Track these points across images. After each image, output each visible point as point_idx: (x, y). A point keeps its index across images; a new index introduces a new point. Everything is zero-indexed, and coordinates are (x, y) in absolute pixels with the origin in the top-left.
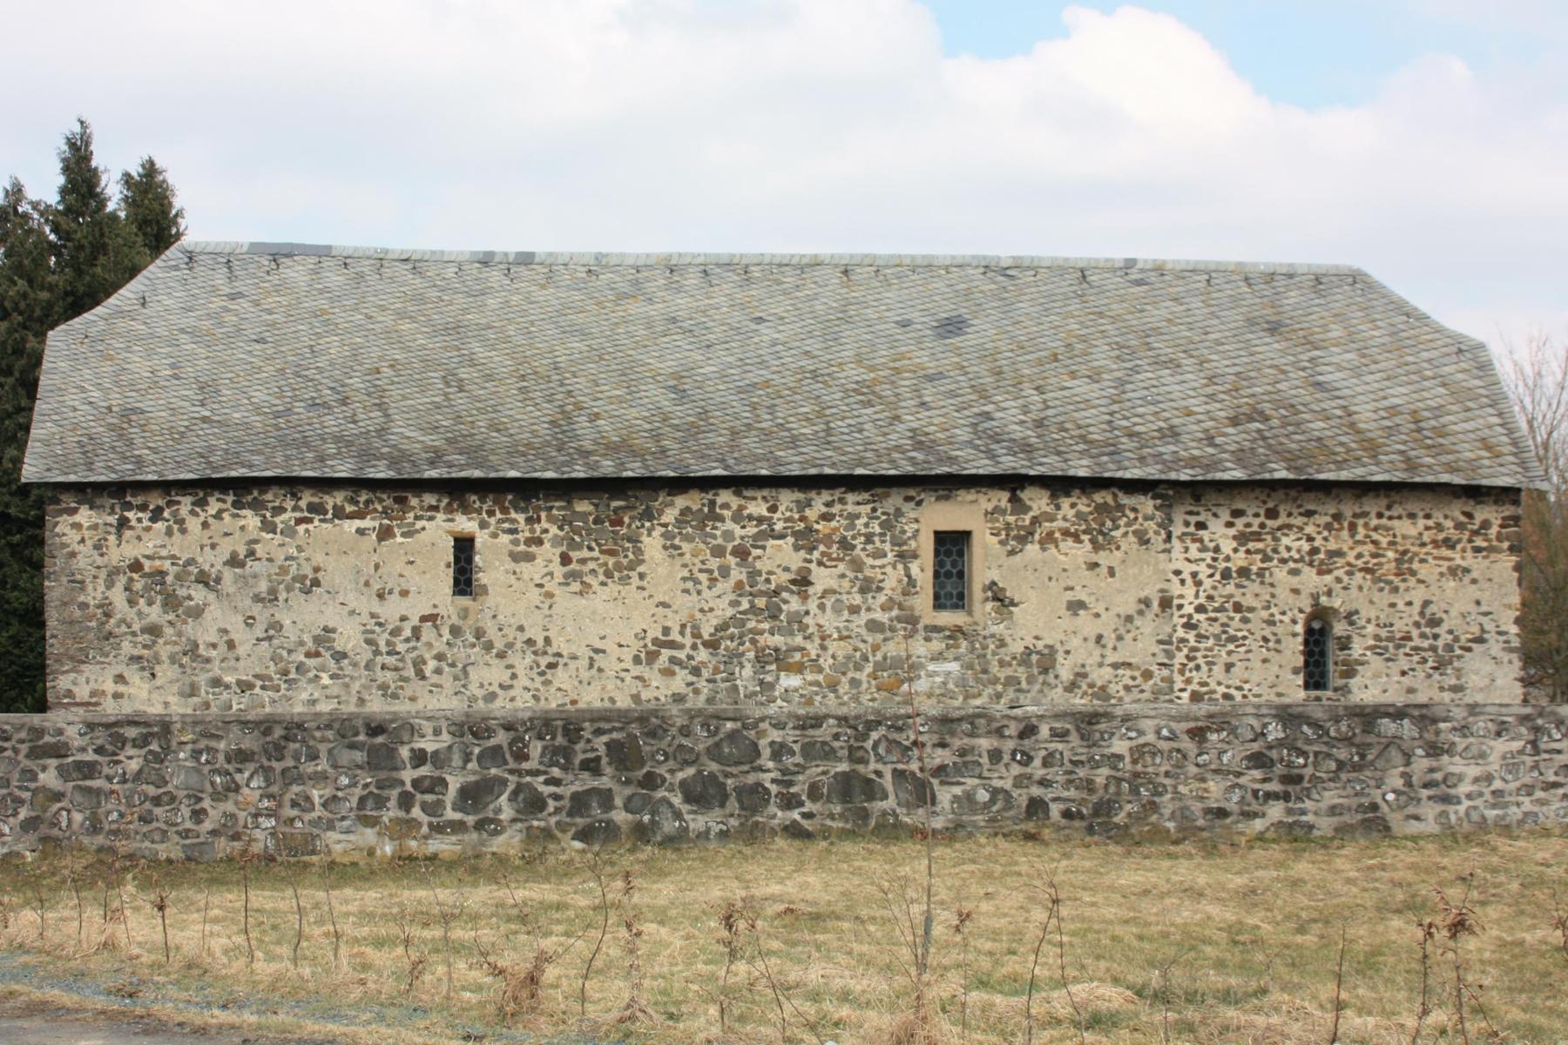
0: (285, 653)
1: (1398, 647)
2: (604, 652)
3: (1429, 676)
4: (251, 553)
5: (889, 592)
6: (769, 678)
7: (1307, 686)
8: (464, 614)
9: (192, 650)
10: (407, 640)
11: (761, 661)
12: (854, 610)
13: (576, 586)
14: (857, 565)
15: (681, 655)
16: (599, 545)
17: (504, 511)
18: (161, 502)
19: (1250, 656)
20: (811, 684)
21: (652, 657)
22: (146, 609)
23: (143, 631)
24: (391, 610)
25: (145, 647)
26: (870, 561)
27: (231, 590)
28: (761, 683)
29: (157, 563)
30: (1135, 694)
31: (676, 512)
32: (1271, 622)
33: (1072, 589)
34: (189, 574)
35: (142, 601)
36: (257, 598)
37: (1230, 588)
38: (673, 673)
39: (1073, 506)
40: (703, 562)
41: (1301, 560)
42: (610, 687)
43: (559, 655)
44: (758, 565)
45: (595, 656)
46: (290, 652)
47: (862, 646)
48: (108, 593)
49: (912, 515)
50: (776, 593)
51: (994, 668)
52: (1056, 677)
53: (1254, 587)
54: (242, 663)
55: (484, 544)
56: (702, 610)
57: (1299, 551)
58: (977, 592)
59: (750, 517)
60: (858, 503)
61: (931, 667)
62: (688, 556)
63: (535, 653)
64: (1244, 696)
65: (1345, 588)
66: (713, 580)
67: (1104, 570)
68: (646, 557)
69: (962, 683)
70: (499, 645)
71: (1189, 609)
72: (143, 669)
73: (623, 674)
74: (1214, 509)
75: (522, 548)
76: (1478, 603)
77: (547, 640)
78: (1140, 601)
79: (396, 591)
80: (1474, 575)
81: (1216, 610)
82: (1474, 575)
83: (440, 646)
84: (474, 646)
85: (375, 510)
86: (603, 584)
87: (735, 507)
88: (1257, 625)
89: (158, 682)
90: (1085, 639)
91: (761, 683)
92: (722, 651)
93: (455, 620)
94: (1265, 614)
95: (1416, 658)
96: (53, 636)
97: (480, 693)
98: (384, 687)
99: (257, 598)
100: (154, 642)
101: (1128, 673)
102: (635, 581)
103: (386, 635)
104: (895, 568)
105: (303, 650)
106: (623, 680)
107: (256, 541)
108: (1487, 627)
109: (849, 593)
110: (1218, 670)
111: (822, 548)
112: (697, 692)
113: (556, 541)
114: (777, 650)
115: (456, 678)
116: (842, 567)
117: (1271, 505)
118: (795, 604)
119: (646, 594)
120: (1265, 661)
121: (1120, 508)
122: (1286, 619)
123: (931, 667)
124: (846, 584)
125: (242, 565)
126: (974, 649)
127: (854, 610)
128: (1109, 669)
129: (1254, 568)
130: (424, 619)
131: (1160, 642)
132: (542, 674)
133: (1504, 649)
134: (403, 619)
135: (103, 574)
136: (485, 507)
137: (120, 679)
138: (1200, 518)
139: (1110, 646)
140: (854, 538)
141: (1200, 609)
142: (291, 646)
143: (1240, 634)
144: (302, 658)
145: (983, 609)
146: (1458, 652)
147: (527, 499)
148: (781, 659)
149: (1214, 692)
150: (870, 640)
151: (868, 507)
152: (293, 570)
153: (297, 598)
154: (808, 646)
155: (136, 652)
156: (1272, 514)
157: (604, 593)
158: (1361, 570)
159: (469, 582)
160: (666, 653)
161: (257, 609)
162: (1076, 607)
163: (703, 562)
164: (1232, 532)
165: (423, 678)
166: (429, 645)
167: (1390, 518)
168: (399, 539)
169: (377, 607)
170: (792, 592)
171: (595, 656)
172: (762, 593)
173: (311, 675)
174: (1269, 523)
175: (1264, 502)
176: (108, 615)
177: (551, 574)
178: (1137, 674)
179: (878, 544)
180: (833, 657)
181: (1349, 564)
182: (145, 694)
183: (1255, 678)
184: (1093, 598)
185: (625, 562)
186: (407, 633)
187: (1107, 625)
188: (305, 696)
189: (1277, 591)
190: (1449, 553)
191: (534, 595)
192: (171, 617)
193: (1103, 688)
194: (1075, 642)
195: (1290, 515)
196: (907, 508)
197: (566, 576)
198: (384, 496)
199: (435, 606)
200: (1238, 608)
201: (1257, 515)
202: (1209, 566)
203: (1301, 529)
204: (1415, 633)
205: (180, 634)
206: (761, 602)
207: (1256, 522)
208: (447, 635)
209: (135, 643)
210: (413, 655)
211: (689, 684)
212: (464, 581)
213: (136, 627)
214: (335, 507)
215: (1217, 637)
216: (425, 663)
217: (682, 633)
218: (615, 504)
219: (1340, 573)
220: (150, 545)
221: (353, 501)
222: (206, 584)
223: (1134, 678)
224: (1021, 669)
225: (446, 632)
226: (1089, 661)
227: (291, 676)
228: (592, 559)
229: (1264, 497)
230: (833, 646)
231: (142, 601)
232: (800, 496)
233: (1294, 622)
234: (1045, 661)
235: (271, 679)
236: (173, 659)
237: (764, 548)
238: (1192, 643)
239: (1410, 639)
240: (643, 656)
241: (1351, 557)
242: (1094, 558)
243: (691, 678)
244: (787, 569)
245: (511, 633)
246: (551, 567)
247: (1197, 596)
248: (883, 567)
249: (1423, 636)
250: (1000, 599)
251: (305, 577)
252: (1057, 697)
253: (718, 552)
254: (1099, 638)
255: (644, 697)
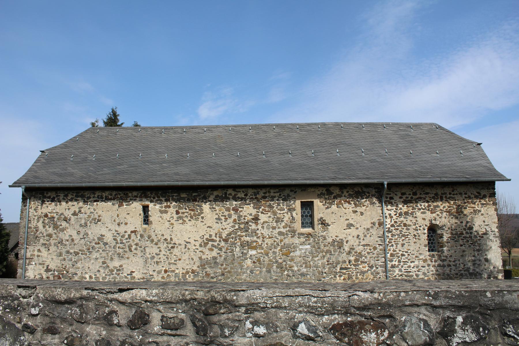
0: (89, 243)
1: (459, 237)
2: (190, 243)
3: (470, 246)
4: (80, 211)
5: (286, 222)
6: (245, 251)
7: (429, 251)
8: (145, 230)
9: (61, 242)
10: (127, 239)
11: (242, 246)
12: (274, 228)
13: (181, 221)
14: (275, 213)
15: (216, 244)
16: (188, 208)
17: (158, 197)
18: (55, 196)
19: (410, 241)
20: (259, 253)
21: (206, 244)
22: (48, 229)
23: (47, 236)
24: (121, 229)
25: (47, 241)
26: (279, 212)
27: (73, 223)
28: (242, 253)
29: (52, 214)
30: (371, 255)
31: (214, 197)
32: (416, 230)
33: (348, 220)
34: (61, 218)
35: (47, 226)
36: (81, 225)
37: (402, 219)
38: (213, 250)
39: (347, 192)
40: (223, 213)
41: (425, 209)
42: (192, 254)
43: (175, 244)
44: (241, 214)
45: (187, 244)
46: (90, 242)
47: (277, 240)
48: (38, 224)
49: (293, 196)
50: (247, 223)
51: (322, 247)
52: (344, 250)
53: (410, 218)
54: (76, 246)
55: (151, 208)
56: (222, 229)
57: (424, 206)
58: (316, 222)
59: (238, 198)
60: (275, 193)
61: (301, 247)
62: (218, 211)
63: (167, 243)
64: (409, 255)
65: (440, 218)
66: (226, 219)
67: (359, 213)
68: (204, 211)
69: (311, 253)
70: (156, 240)
71: (388, 226)
72: (46, 248)
73: (196, 250)
74: (396, 193)
75: (164, 209)
76: (484, 222)
77: (171, 239)
78: (372, 223)
79: (124, 223)
80: (482, 212)
81: (398, 226)
82: (482, 212)
83: (137, 241)
84: (148, 241)
85: (118, 197)
86: (190, 220)
87: (233, 195)
88: (411, 231)
89: (50, 252)
90: (353, 237)
91: (242, 253)
92: (229, 242)
93: (142, 232)
94: (414, 227)
95: (465, 240)
96: (21, 237)
97: (149, 256)
98: (119, 254)
99: (81, 225)
100: (50, 239)
101: (369, 248)
102: (200, 219)
103: (120, 237)
104: (287, 214)
105: (94, 242)
106: (196, 252)
107: (82, 208)
108: (488, 230)
109: (272, 222)
110: (399, 246)
111: (263, 207)
112: (221, 256)
113: (174, 207)
114: (247, 242)
115: (142, 251)
116: (269, 213)
117: (414, 191)
118: (253, 226)
119: (204, 223)
120: (415, 243)
121: (364, 192)
122: (421, 228)
123: (301, 247)
124: (271, 219)
125: (77, 215)
126: (315, 241)
127: (274, 228)
128: (362, 247)
129: (410, 212)
130: (132, 232)
131: (379, 237)
132: (170, 250)
133: (494, 237)
134: (126, 232)
135: (36, 218)
136: (152, 196)
137: (39, 250)
138: (391, 196)
139: (362, 239)
140: (273, 204)
141: (392, 226)
142: (91, 241)
143: (406, 234)
144: (94, 244)
145: (318, 227)
146: (479, 238)
147: (443, 188)
148: (250, 245)
149: (398, 253)
150: (279, 238)
151: (278, 194)
152: (92, 217)
153: (93, 225)
154: (258, 240)
155: (44, 242)
156: (415, 194)
157: (190, 223)
158: (445, 212)
159: (148, 220)
160: (210, 243)
161: (81, 229)
162: (350, 226)
163: (223, 213)
164: (402, 200)
165: (131, 251)
166: (133, 240)
167: (454, 194)
168: (125, 206)
169: (117, 228)
170: (253, 223)
171: (187, 244)
172: (242, 223)
173: (96, 250)
174: (414, 197)
175: (412, 190)
176: (37, 231)
177: (173, 217)
178: (371, 248)
179: (282, 206)
180: (267, 244)
181: (441, 210)
182: (46, 255)
183: (412, 249)
184: (355, 223)
185: (197, 213)
186: (127, 236)
187: (361, 232)
188: (94, 257)
189: (418, 219)
190: (473, 206)
191: (167, 224)
192: (55, 231)
193: (360, 253)
194: (350, 238)
195: (421, 194)
196: (291, 194)
197: (178, 218)
198: (121, 193)
199: (136, 228)
200: (405, 225)
201: (410, 194)
202: (395, 211)
203: (425, 199)
204: (464, 232)
205: (57, 237)
206: (242, 226)
207: (410, 196)
208: (139, 237)
209: (44, 240)
210: (129, 244)
211: (218, 254)
212: (146, 220)
213: (45, 234)
214: (106, 196)
215: (398, 235)
216: (132, 246)
217: (216, 237)
218: (194, 194)
219: (438, 213)
220: (51, 209)
221: (111, 195)
222: (66, 221)
223: (370, 250)
224: (331, 247)
225: (139, 236)
226: (355, 244)
227: (91, 250)
228: (186, 212)
229: (411, 188)
230: (267, 241)
231: (47, 226)
232: (256, 191)
233: (424, 229)
234: (339, 244)
235: (84, 251)
236: (55, 245)
237: (243, 208)
238: (390, 237)
239: (463, 234)
240: (203, 244)
241: (441, 207)
242: (355, 209)
243: (219, 252)
244: (251, 215)
245: (160, 237)
246: (173, 215)
247: (391, 221)
248: (284, 213)
249: (467, 233)
250: (324, 224)
251: (96, 219)
252: (344, 256)
253: (228, 210)
254: (358, 236)
255: (203, 258)
